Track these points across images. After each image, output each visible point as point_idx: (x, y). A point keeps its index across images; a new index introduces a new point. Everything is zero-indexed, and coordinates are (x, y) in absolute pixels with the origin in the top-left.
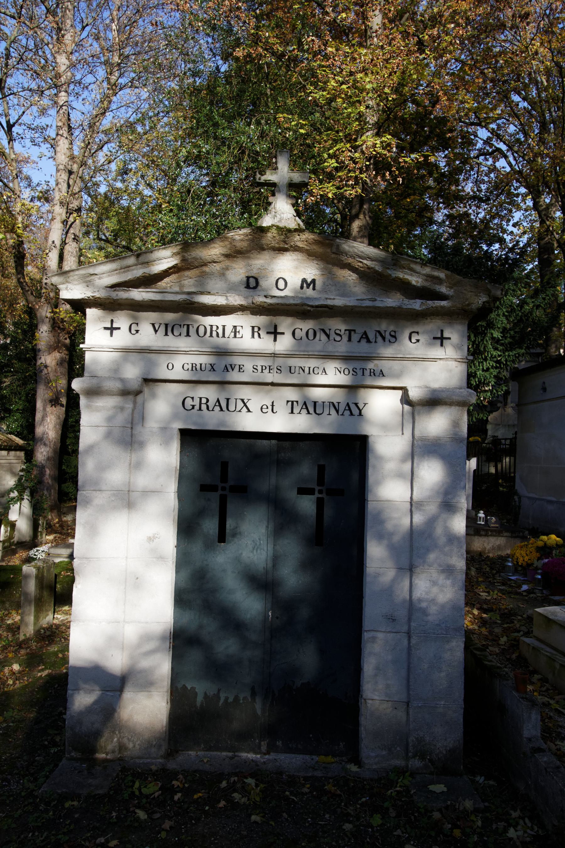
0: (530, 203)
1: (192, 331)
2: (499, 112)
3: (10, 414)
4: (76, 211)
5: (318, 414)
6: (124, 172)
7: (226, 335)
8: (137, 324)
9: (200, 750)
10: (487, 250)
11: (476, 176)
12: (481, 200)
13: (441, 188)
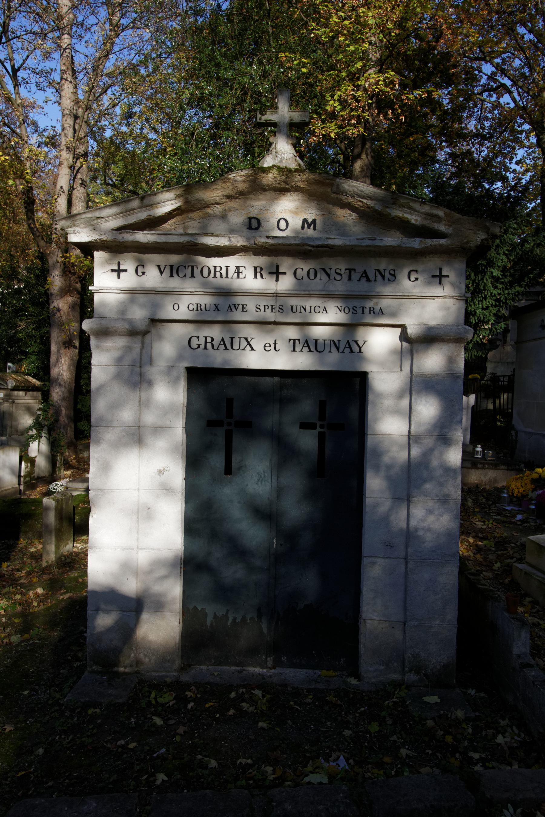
0: (533, 140)
1: (197, 272)
2: (504, 45)
3: (26, 356)
4: (82, 156)
5: (320, 352)
6: (129, 115)
7: (230, 276)
8: (143, 266)
9: (211, 665)
10: (489, 188)
11: (479, 112)
12: (484, 138)
13: (444, 126)
